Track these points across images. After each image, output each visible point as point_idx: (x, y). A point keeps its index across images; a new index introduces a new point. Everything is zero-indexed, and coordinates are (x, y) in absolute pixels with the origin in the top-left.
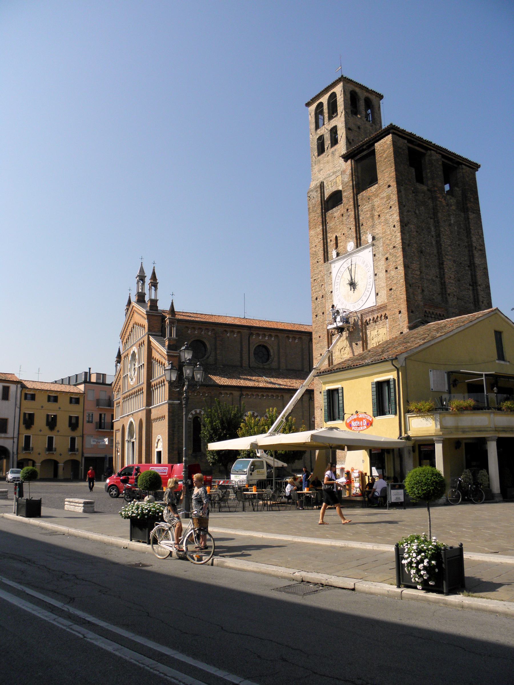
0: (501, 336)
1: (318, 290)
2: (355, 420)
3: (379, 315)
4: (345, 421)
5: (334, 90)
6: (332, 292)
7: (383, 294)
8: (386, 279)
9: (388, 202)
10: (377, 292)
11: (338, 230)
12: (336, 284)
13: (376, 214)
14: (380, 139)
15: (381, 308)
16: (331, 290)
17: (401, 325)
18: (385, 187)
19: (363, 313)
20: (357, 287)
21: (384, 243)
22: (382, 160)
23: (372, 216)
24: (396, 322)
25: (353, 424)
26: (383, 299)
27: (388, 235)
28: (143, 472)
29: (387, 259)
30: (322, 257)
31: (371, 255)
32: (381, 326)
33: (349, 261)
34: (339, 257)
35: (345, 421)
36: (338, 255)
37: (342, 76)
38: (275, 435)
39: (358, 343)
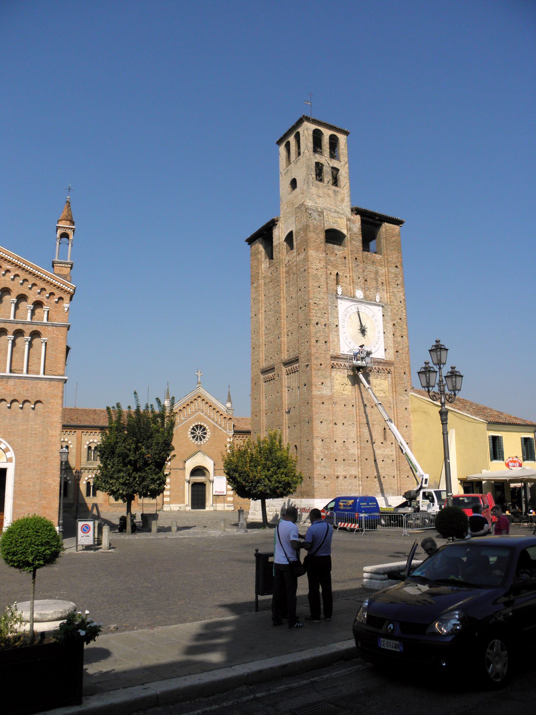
1: (319, 315)
2: (511, 462)
6: (337, 326)
7: (392, 351)
15: (387, 363)
23: (377, 280)
24: (402, 380)
25: (511, 464)
26: (390, 356)
29: (394, 325)
38: (222, 460)
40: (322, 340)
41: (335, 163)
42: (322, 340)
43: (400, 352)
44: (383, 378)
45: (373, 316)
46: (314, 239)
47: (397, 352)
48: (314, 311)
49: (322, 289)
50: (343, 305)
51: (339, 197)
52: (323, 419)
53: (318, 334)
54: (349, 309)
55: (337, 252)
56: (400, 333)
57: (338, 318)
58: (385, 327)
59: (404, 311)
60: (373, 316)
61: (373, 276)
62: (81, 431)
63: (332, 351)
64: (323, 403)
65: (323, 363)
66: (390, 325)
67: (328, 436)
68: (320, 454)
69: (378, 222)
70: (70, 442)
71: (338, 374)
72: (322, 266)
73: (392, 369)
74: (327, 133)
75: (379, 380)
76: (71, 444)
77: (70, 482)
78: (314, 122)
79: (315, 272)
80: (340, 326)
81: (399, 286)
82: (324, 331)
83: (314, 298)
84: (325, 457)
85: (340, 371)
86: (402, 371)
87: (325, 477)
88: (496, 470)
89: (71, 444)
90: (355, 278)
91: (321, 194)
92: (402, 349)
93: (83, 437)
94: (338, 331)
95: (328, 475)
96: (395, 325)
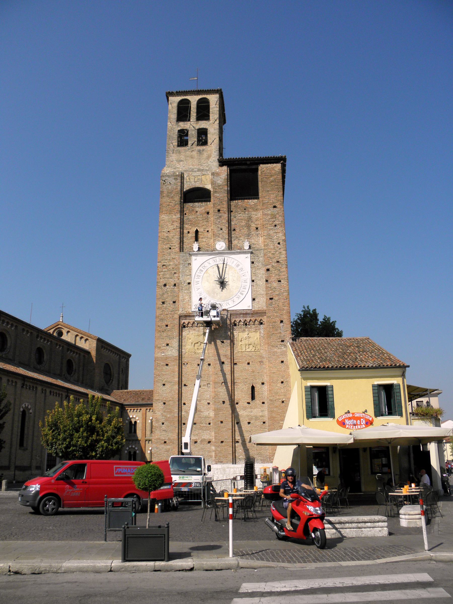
0: (128, 361)
1: (168, 276)
2: (350, 419)
3: (253, 319)
4: (336, 419)
5: (208, 97)
6: (189, 283)
8: (266, 288)
9: (273, 220)
10: (254, 297)
11: (200, 225)
12: (196, 277)
14: (268, 163)
15: (257, 313)
16: (189, 281)
17: (283, 334)
18: (270, 206)
20: (227, 287)
21: (265, 255)
22: (269, 181)
23: (249, 227)
24: (277, 330)
25: (347, 422)
26: (261, 304)
27: (271, 249)
29: (268, 270)
30: (178, 246)
31: (248, 261)
32: (253, 330)
35: (336, 419)
36: (199, 249)
37: (221, 90)
39: (225, 341)
40: (169, 301)
41: (203, 124)
42: (169, 301)
43: (276, 298)
44: (253, 330)
45: (238, 266)
46: (168, 204)
47: (271, 299)
48: (162, 273)
49: (173, 250)
50: (197, 262)
51: (205, 154)
52: (166, 381)
53: (165, 296)
54: (206, 264)
55: (197, 209)
56: (277, 277)
57: (190, 275)
58: (253, 273)
59: (284, 252)
60: (240, 267)
61: (243, 223)
62: (145, 408)
64: (167, 365)
65: (169, 323)
66: (262, 272)
67: (171, 399)
68: (160, 417)
69: (254, 167)
70: (137, 418)
71: (191, 333)
72: (175, 227)
73: (265, 319)
74: (194, 100)
75: (247, 333)
76: (138, 420)
77: (138, 452)
78: (178, 93)
79: (166, 235)
80: (192, 284)
81: (278, 227)
83: (162, 260)
84: (166, 420)
85: (194, 330)
86: (278, 320)
87: (165, 442)
88: (326, 432)
89: (138, 420)
91: (182, 157)
92: (278, 295)
93: (148, 413)
94: (189, 289)
95: (169, 439)
96: (266, 270)
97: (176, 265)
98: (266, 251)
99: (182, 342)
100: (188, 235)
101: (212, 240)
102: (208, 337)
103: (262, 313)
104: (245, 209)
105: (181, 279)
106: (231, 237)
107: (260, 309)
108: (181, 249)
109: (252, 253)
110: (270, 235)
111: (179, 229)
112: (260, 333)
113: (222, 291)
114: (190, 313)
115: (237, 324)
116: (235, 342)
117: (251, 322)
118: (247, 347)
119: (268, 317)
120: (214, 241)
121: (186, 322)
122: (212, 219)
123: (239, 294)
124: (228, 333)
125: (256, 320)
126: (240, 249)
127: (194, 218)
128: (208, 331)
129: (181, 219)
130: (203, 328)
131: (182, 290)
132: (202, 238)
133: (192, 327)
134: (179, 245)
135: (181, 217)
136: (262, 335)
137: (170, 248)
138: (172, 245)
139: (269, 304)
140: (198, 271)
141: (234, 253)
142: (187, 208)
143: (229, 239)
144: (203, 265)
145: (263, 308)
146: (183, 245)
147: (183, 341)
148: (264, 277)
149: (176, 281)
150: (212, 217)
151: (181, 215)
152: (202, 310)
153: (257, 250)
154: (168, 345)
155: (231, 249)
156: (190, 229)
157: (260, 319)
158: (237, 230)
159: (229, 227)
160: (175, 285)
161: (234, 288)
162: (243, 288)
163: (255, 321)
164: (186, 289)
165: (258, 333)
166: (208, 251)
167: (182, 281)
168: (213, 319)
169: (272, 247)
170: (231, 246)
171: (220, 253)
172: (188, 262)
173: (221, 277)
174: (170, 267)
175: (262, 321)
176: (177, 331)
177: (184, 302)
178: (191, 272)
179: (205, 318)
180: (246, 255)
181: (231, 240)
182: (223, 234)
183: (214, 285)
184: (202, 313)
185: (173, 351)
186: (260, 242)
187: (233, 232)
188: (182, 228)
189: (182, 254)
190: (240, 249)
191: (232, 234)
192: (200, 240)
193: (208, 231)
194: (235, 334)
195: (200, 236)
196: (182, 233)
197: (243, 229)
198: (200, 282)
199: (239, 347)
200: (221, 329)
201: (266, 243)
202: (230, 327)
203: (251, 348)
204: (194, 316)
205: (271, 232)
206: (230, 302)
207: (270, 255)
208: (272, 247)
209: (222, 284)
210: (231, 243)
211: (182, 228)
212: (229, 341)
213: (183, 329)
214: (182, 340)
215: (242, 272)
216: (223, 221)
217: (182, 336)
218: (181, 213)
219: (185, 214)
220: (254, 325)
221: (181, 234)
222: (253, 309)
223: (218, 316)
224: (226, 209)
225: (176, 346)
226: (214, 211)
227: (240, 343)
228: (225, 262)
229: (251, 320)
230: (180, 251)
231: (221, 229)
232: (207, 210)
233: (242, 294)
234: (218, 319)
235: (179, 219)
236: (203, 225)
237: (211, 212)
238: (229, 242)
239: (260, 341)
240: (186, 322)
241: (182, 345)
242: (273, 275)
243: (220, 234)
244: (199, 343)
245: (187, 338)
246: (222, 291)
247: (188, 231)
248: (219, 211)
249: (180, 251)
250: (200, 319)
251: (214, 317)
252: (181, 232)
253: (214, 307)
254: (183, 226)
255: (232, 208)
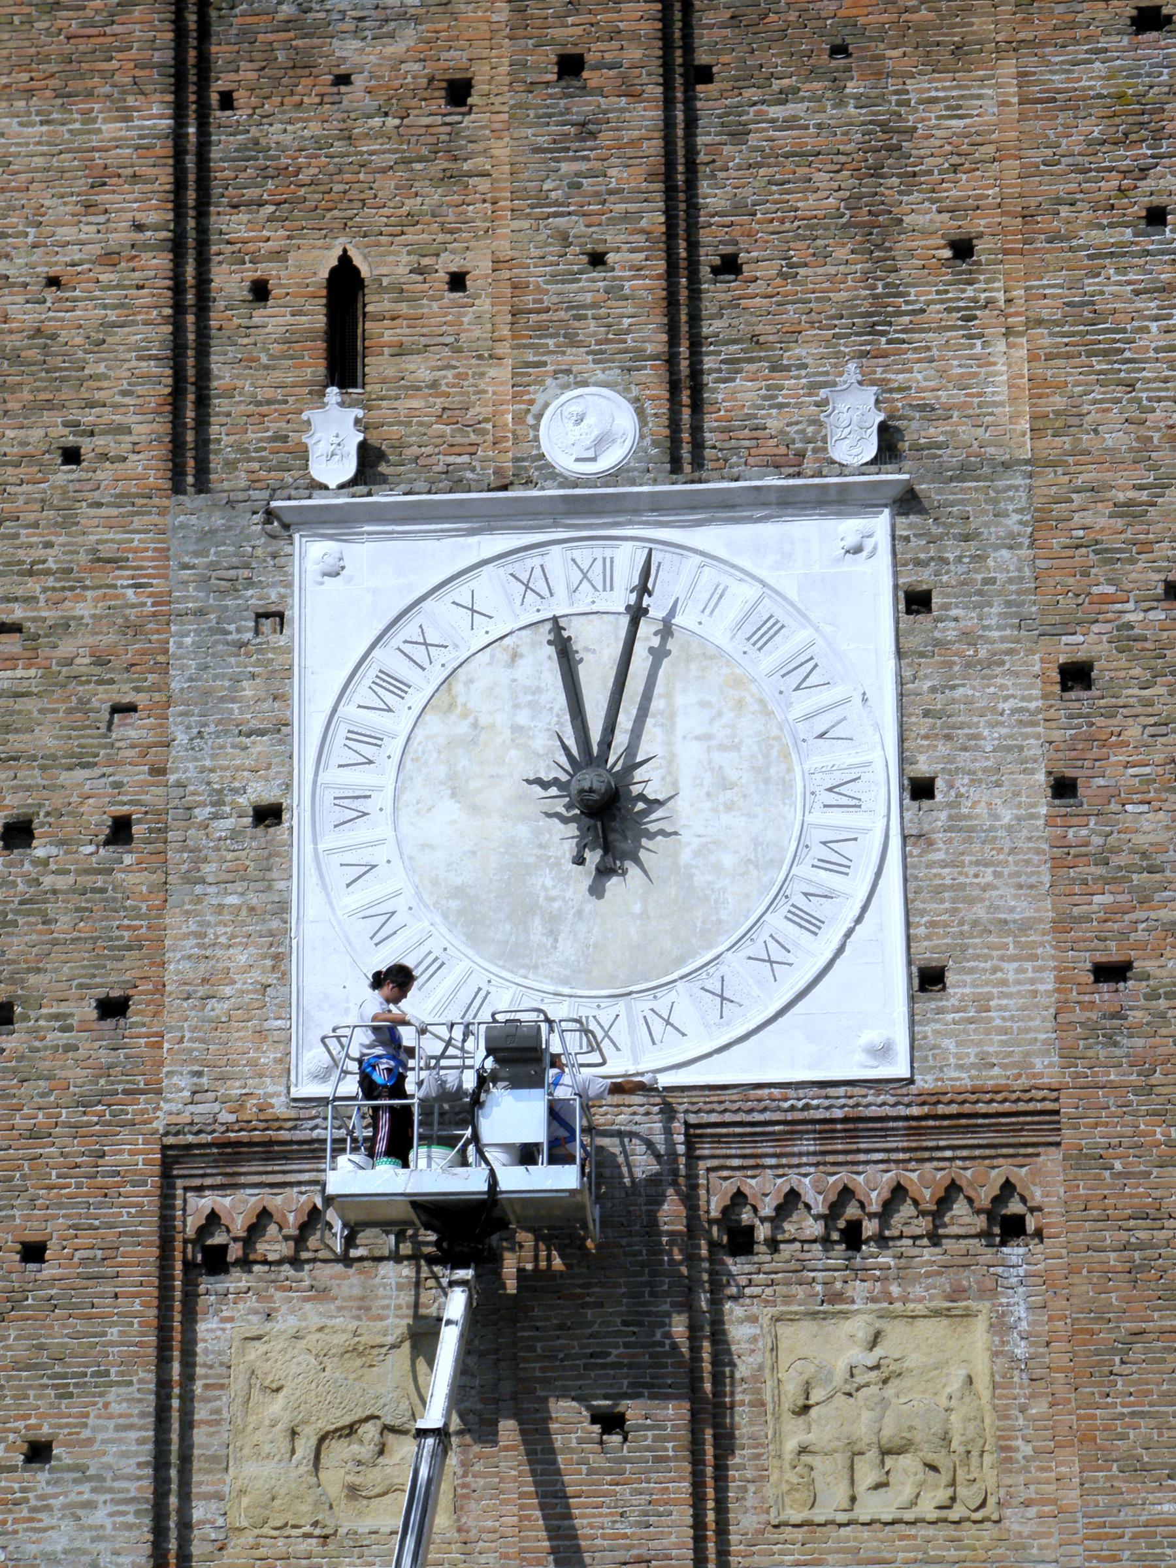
1: (46, 739)
3: (924, 1181)
6: (268, 815)
8: (1057, 864)
9: (1125, 157)
10: (929, 956)
11: (376, 218)
12: (339, 752)
13: (925, 222)
16: (261, 792)
19: (716, 1123)
20: (653, 853)
21: (1042, 520)
23: (875, 232)
26: (1011, 1029)
27: (1111, 460)
28: (1031, 1318)
29: (1076, 675)
30: (147, 428)
31: (875, 585)
32: (924, 1294)
33: (626, 561)
34: (382, 498)
36: (370, 464)
39: (633, 1410)
44: (924, 1294)
45: (765, 633)
47: (1111, 973)
49: (105, 473)
50: (347, 593)
54: (442, 616)
57: (280, 728)
58: (920, 713)
60: (789, 637)
61: (823, 196)
63: (180, 1083)
65: (54, 1229)
66: (1013, 697)
71: (286, 1322)
72: (121, 237)
73: (1046, 1183)
75: (858, 1326)
80: (299, 816)
82: (93, 897)
85: (320, 1293)
90: (536, 276)
97: (133, 629)
98: (1051, 481)
99: (187, 1424)
100: (259, 315)
101: (502, 373)
102: (463, 1369)
103: (1014, 1120)
104: (839, 50)
105: (183, 769)
106: (696, 343)
107: (995, 1077)
108: (188, 461)
109: (907, 502)
110: (1098, 317)
111: (162, 261)
112: (1000, 1326)
113: (597, 891)
114: (277, 1122)
115: (762, 1232)
116: (743, 1422)
117: (907, 1210)
118: (867, 1474)
119: (1080, 1160)
120: (521, 385)
121: (236, 1208)
122: (501, 149)
123: (776, 921)
124: (662, 1322)
125: (953, 1189)
126: (790, 460)
127: (320, 144)
128: (456, 1305)
129: (179, 153)
130: (406, 1271)
131: (193, 879)
132: (401, 351)
133: (295, 1262)
134: (162, 426)
135: (178, 135)
136: (1021, 1350)
137: (71, 456)
138: (88, 418)
139: (1092, 1029)
140: (362, 693)
141: (726, 508)
142: (247, 35)
143: (671, 360)
144: (409, 629)
145: (1024, 1064)
146: (202, 423)
147: (201, 1412)
148: (1034, 748)
149: (136, 791)
150: (497, 137)
151: (179, 113)
152: (397, 1090)
153: (965, 472)
154: (38, 1452)
155: (698, 462)
156: (279, 255)
157: (996, 1178)
158: (762, 267)
159: (671, 234)
160: (120, 831)
161: (728, 860)
162: (823, 864)
163: (944, 1202)
164: (235, 876)
165: (980, 1326)
166: (458, 485)
167: (198, 792)
168: (515, 1180)
169: (1116, 438)
170: (697, 430)
171: (588, 507)
172: (253, 599)
173: (587, 757)
174: (66, 648)
175: (1015, 1207)
176: (141, 1308)
177: (217, 1008)
178: (280, 697)
179: (432, 1173)
180: (849, 528)
181: (696, 373)
182: (618, 308)
183: (523, 831)
184: (401, 1118)
185: (99, 1516)
186: (998, 390)
187: (714, 292)
188: (189, 243)
189: (192, 513)
190: (790, 460)
191: (708, 307)
192: (377, 366)
193: (457, 281)
194: (739, 1333)
195: (378, 335)
196: (190, 301)
197: (824, 256)
198: (383, 799)
199: (782, 1476)
200: (598, 1281)
201: (1058, 401)
202: (691, 1258)
203: (908, 1489)
204: (313, 1151)
205: (1111, 286)
206: (685, 1003)
207: (1100, 519)
208: (1116, 438)
209: (608, 816)
210: (697, 406)
211: (189, 243)
212: (675, 1413)
213: (205, 1284)
214: (187, 1398)
215: (804, 703)
216: (617, 175)
217: (189, 1363)
218: (179, 88)
219: (227, 101)
220: (935, 1239)
221: (179, 308)
222: (925, 1082)
223: (559, 1157)
224: (640, 54)
225: (129, 1466)
226: (518, 66)
227: (794, 1435)
228: (657, 607)
229: (899, 1192)
230: (178, 488)
231: (597, 260)
232: (454, 60)
233: (812, 925)
234: (564, 1178)
235: (164, 148)
236: (412, 219)
237: (491, 76)
238: (674, 387)
239: (1002, 1414)
240: (236, 1208)
241: (186, 1459)
242: (1133, 732)
243: (578, 311)
244: (370, 1431)
245: (238, 1385)
246: (597, 891)
247: (252, 273)
248: (570, 66)
249: (178, 488)
250: (384, 1179)
251: (526, 1155)
252: (178, 288)
253: (520, 1056)
254: (203, 231)
255: (704, 38)
